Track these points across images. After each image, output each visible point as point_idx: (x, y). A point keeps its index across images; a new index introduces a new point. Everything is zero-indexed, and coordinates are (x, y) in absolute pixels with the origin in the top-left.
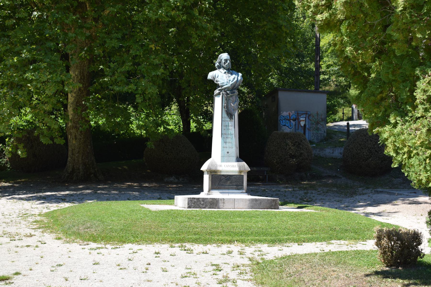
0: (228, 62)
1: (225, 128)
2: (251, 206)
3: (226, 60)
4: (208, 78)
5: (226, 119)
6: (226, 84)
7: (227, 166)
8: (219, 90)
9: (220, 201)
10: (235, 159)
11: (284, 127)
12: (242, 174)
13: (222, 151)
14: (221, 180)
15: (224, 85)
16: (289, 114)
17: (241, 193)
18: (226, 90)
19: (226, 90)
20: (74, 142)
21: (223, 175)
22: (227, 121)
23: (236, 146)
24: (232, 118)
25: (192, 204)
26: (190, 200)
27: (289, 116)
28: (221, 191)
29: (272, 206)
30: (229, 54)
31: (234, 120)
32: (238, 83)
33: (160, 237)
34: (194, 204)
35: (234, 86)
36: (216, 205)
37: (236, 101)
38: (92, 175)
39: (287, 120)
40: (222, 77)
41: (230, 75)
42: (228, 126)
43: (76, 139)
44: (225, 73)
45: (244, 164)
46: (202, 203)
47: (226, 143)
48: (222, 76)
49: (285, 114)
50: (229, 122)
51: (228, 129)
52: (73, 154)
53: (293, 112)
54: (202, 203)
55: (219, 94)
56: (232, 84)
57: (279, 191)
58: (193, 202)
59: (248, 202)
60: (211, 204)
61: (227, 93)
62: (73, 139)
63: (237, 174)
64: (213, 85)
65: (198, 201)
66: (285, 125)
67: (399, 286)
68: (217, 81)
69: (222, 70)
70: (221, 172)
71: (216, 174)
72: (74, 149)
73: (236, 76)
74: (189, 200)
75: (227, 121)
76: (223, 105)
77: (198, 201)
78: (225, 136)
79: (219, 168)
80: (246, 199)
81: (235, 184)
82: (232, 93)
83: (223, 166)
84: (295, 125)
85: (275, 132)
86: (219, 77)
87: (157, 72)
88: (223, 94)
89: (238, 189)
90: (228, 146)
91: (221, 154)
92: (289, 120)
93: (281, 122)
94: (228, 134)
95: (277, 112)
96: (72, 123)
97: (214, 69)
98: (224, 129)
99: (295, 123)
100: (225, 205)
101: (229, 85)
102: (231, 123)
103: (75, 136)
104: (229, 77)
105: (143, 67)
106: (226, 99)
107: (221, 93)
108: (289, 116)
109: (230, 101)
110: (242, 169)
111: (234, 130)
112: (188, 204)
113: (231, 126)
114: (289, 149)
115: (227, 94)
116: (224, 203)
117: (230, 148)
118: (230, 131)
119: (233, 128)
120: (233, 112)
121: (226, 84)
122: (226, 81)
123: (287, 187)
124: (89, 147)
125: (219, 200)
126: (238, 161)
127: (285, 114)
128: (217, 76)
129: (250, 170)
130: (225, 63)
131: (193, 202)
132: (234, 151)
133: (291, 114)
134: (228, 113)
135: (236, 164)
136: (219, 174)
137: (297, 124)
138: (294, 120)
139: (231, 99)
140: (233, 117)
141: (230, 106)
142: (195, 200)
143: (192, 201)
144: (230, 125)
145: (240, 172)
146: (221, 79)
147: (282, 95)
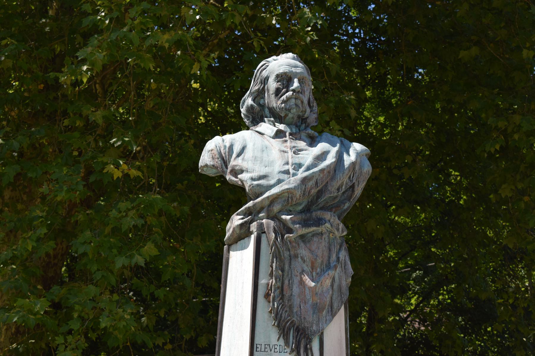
3: (285, 79)
4: (201, 163)
6: (279, 182)
8: (248, 212)
15: (270, 187)
18: (276, 208)
19: (276, 208)
32: (342, 179)
35: (320, 193)
37: (329, 267)
44: (279, 134)
48: (264, 149)
55: (243, 232)
56: (304, 180)
61: (283, 223)
64: (224, 194)
67: (212, 1)
68: (236, 172)
69: (267, 127)
73: (334, 150)
76: (263, 281)
82: (305, 224)
86: (248, 154)
87: (131, 257)
97: (237, 126)
101: (290, 183)
105: (84, 244)
106: (277, 255)
107: (254, 227)
109: (298, 264)
115: (283, 229)
121: (279, 182)
122: (278, 166)
130: (278, 93)
139: (303, 251)
140: (315, 345)
141: (296, 290)
146: (255, 158)
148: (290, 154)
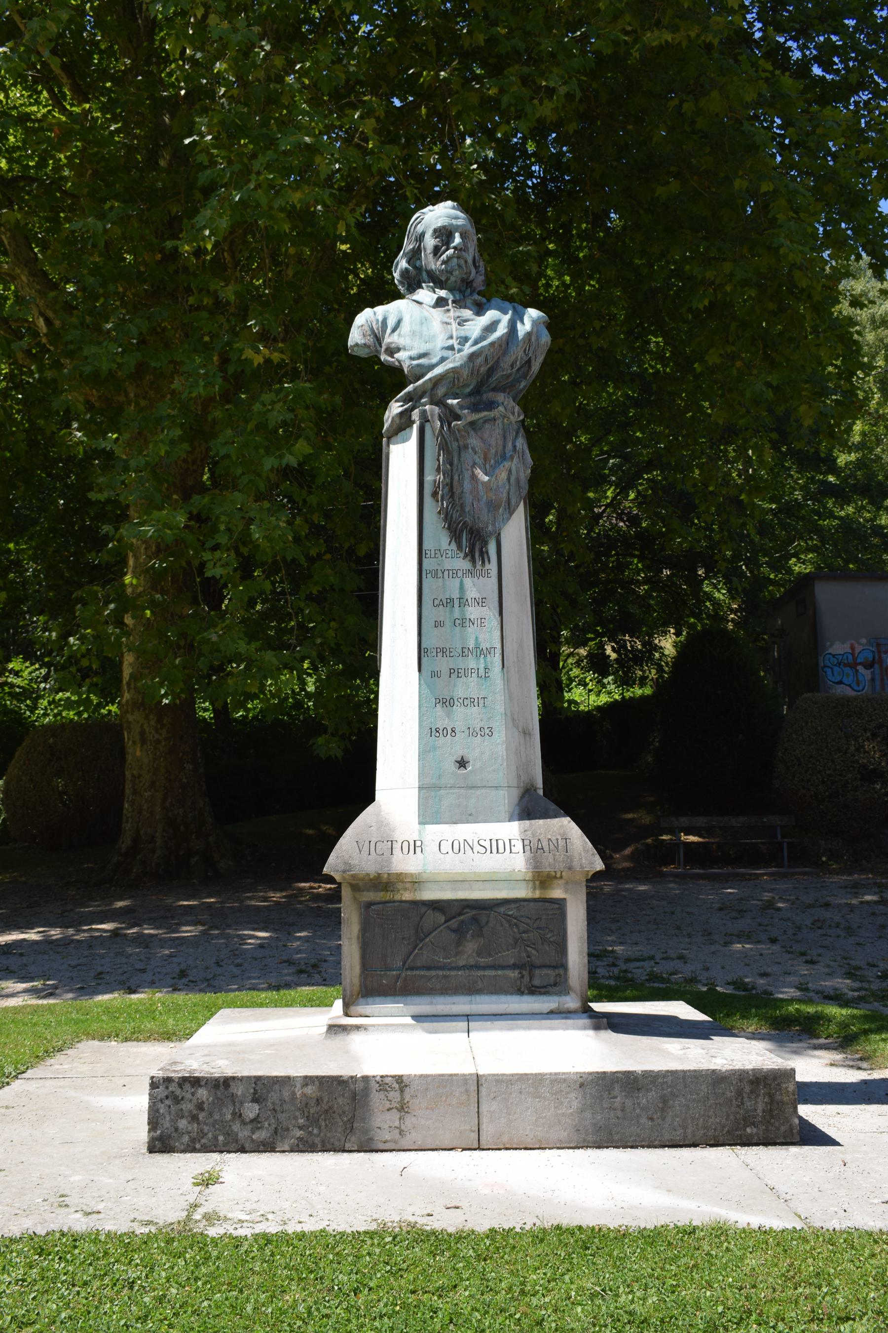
0: (457, 240)
1: (441, 613)
2: (598, 1129)
3: (444, 234)
4: (350, 343)
5: (448, 564)
6: (443, 360)
7: (458, 848)
8: (408, 398)
9: (377, 1099)
10: (506, 799)
11: (837, 686)
12: (557, 893)
13: (425, 753)
14: (420, 935)
15: (432, 367)
16: (852, 648)
17: (553, 1014)
18: (441, 391)
19: (441, 391)
20: (138, 753)
21: (436, 906)
22: (454, 573)
23: (514, 720)
24: (484, 556)
25: (183, 1124)
27: (853, 654)
28: (424, 1005)
29: (748, 1121)
30: (464, 207)
31: (493, 566)
34: (194, 1118)
35: (491, 371)
36: (350, 1128)
38: (196, 859)
39: (845, 665)
40: (420, 328)
41: (467, 313)
42: (463, 602)
43: (143, 742)
44: (440, 303)
45: (566, 830)
46: (251, 1110)
47: (447, 702)
48: (424, 321)
49: (839, 648)
50: (468, 582)
51: (463, 622)
52: (135, 792)
53: (864, 641)
54: (251, 1110)
55: (404, 423)
56: (472, 357)
57: (827, 905)
58: (187, 1106)
59: (573, 1102)
60: (313, 1121)
62: (134, 742)
63: (521, 892)
64: (380, 378)
65: (219, 1103)
66: (840, 682)
68: (391, 351)
69: (426, 295)
70: (416, 882)
71: (388, 896)
72: (140, 776)
73: (506, 319)
74: (161, 1092)
75: (454, 573)
76: (429, 478)
77: (219, 1103)
78: (443, 664)
79: (406, 864)
80: (555, 1084)
81: (510, 956)
82: (475, 408)
83: (431, 847)
84: (873, 680)
85: (806, 695)
86: (405, 328)
87: (281, 457)
88: (425, 419)
89: (533, 991)
90: (459, 726)
91: (422, 774)
92: (853, 666)
93: (828, 670)
94: (464, 652)
95: (814, 642)
96: (132, 691)
98: (438, 624)
99: (873, 673)
100: (409, 1121)
101: (456, 361)
102: (478, 586)
103: (142, 733)
104: (462, 322)
105: (226, 443)
106: (444, 446)
107: (416, 415)
108: (853, 654)
109: (468, 456)
110: (549, 863)
111: (495, 623)
112: (154, 1122)
113: (481, 602)
114: (857, 750)
115: (449, 415)
116: (403, 1108)
117: (472, 732)
118: (471, 631)
119: (490, 613)
120: (485, 517)
121: (443, 360)
122: (441, 341)
123: (856, 888)
124: (189, 767)
125: (366, 1091)
126: (527, 809)
127: (839, 648)
128: (391, 323)
129: (599, 865)
130: (436, 251)
131: (187, 1106)
132: (501, 750)
133: (858, 649)
134: (462, 528)
135: (511, 830)
136: (407, 896)
137: (878, 677)
138: (869, 665)
139: (474, 441)
140: (492, 548)
141: (467, 486)
142: (202, 1093)
143: (177, 1100)
144: (472, 593)
145: (542, 878)
147: (826, 594)
148: (454, 325)
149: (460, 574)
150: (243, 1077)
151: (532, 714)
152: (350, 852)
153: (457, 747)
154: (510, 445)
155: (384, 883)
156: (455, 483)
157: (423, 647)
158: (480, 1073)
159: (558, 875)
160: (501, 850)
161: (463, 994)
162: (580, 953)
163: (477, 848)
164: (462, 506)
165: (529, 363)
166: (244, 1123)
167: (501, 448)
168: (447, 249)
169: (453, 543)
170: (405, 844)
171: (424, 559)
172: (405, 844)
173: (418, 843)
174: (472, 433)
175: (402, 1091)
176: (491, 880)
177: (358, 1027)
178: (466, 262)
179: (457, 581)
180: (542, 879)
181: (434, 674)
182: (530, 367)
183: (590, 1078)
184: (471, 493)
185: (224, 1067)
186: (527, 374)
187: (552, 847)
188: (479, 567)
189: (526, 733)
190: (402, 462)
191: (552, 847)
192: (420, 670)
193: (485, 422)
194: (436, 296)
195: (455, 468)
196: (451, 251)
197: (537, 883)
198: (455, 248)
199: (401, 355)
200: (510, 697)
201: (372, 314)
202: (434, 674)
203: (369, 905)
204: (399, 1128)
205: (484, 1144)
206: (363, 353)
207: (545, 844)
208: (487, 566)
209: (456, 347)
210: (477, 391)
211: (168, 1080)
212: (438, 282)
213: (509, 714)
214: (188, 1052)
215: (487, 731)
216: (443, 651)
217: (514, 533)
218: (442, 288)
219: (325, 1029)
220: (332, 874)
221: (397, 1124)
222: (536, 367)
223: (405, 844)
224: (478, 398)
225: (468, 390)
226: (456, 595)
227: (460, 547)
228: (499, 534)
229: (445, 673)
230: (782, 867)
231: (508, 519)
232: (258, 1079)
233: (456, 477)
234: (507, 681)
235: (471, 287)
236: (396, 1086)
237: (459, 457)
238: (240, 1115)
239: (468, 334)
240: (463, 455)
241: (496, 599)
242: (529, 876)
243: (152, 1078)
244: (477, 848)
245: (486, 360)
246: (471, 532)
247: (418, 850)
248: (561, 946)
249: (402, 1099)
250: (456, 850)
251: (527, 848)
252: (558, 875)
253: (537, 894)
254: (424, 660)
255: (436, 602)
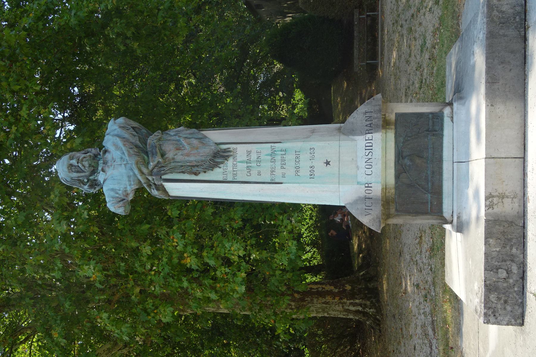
1: (254, 172)
5: (230, 168)
9: (497, 210)
15: (134, 174)
23: (307, 138)
24: (225, 151)
26: (492, 314)
31: (232, 146)
33: (444, 55)
35: (137, 146)
40: (117, 180)
50: (239, 159)
54: (503, 274)
59: (500, 108)
70: (385, 189)
74: (492, 319)
75: (234, 166)
86: (116, 187)
90: (309, 164)
98: (259, 174)
113: (249, 153)
116: (502, 196)
121: (131, 169)
132: (321, 144)
149: (235, 163)
150: (485, 277)
151: (304, 129)
152: (369, 219)
153: (319, 165)
154: (173, 138)
155: (386, 202)
156: (191, 164)
157: (270, 181)
158: (485, 156)
159: (384, 116)
160: (371, 144)
161: (442, 164)
162: (423, 106)
163: (369, 156)
164: (202, 161)
165: (133, 128)
166: (508, 277)
167: (174, 142)
168: (78, 166)
169: (220, 166)
170: (367, 192)
171: (228, 180)
172: (367, 192)
173: (367, 185)
174: (167, 156)
175: (493, 197)
176: (385, 149)
177: (458, 218)
178: (84, 157)
179: (238, 164)
180: (386, 124)
181: (284, 176)
182: (136, 127)
183: (488, 101)
184: (196, 157)
185: (478, 286)
186: (138, 128)
187: (369, 120)
188: (232, 153)
189: (313, 131)
190: (176, 190)
191: (369, 120)
192: (281, 183)
193: (161, 149)
194: (101, 172)
195: (184, 164)
196: (80, 165)
197: (387, 127)
198: (78, 163)
199: (129, 189)
200: (295, 139)
201: (110, 203)
202: (284, 176)
203: (397, 210)
204: (513, 198)
205: (522, 156)
206: (129, 208)
207: (368, 123)
208: (232, 149)
209: (125, 163)
210: (147, 153)
211: (485, 314)
212: (94, 171)
213: (304, 140)
214: (469, 302)
215: (312, 151)
216: (272, 172)
217: (216, 136)
218: (98, 169)
219: (459, 234)
220: (381, 228)
221: (511, 199)
222: (135, 124)
223: (367, 192)
224: (149, 153)
225: (146, 157)
226: (245, 165)
227: (222, 163)
228: (216, 143)
229: (283, 171)
230: (378, 14)
231: (209, 139)
232: (486, 269)
233: (188, 164)
234: (288, 140)
235: (97, 155)
236: (490, 200)
237: (179, 162)
238: (504, 279)
239: (120, 157)
240: (177, 160)
241: (247, 145)
242: (384, 131)
243: (484, 323)
244: (369, 156)
245: (131, 148)
246: (214, 157)
247: (370, 185)
248: (420, 115)
249: (498, 196)
250: (370, 167)
251: (370, 131)
252: (384, 116)
253: (393, 127)
254: (277, 181)
255: (249, 174)
